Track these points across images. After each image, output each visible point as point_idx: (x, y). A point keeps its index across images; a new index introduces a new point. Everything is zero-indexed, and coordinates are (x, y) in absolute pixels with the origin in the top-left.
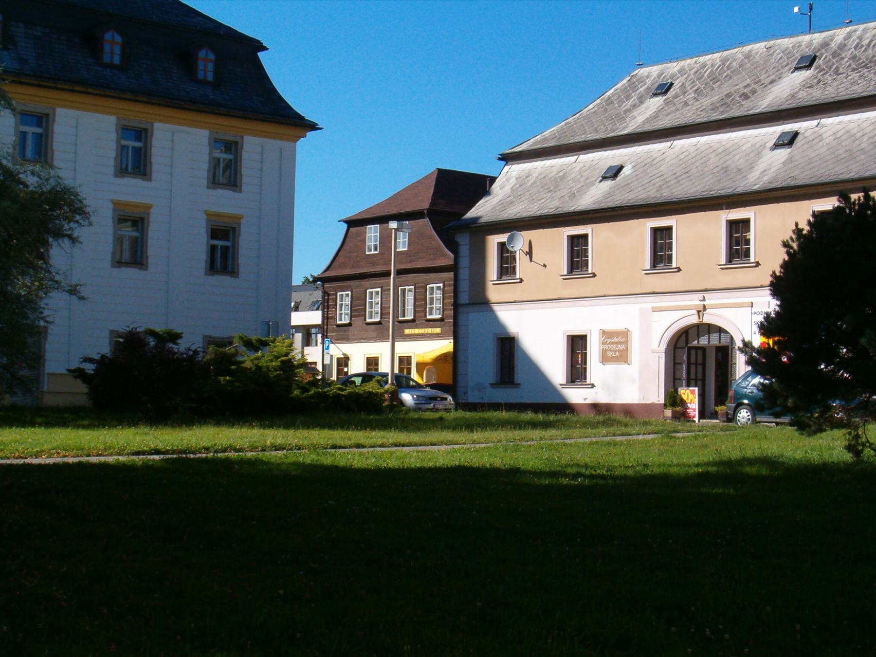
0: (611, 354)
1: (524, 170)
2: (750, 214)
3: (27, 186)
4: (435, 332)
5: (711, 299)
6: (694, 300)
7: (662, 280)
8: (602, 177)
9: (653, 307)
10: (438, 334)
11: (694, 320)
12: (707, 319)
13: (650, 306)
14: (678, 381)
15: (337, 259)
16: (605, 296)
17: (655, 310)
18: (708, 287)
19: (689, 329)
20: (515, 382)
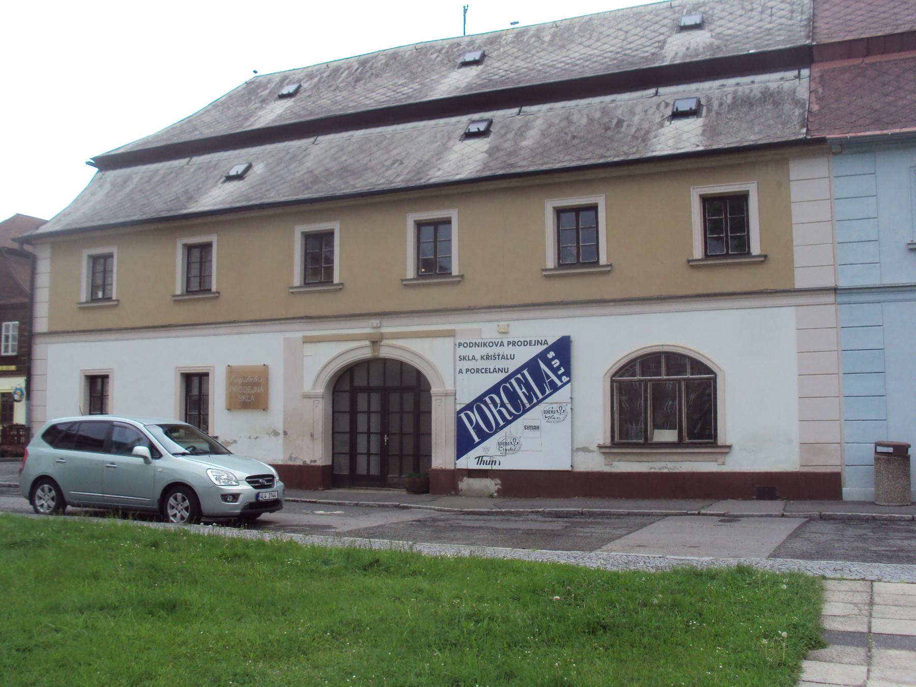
0: (244, 398)
1: (300, 147)
2: (749, 185)
3: (244, 94)
4: (10, 369)
5: (389, 327)
6: (364, 328)
7: (201, 310)
8: (226, 177)
9: (304, 337)
10: (13, 371)
11: (366, 353)
12: (385, 352)
13: (300, 335)
14: (337, 434)
15: (438, 235)
16: (234, 322)
17: (307, 340)
18: (172, 322)
19: (354, 366)
20: (720, 441)
